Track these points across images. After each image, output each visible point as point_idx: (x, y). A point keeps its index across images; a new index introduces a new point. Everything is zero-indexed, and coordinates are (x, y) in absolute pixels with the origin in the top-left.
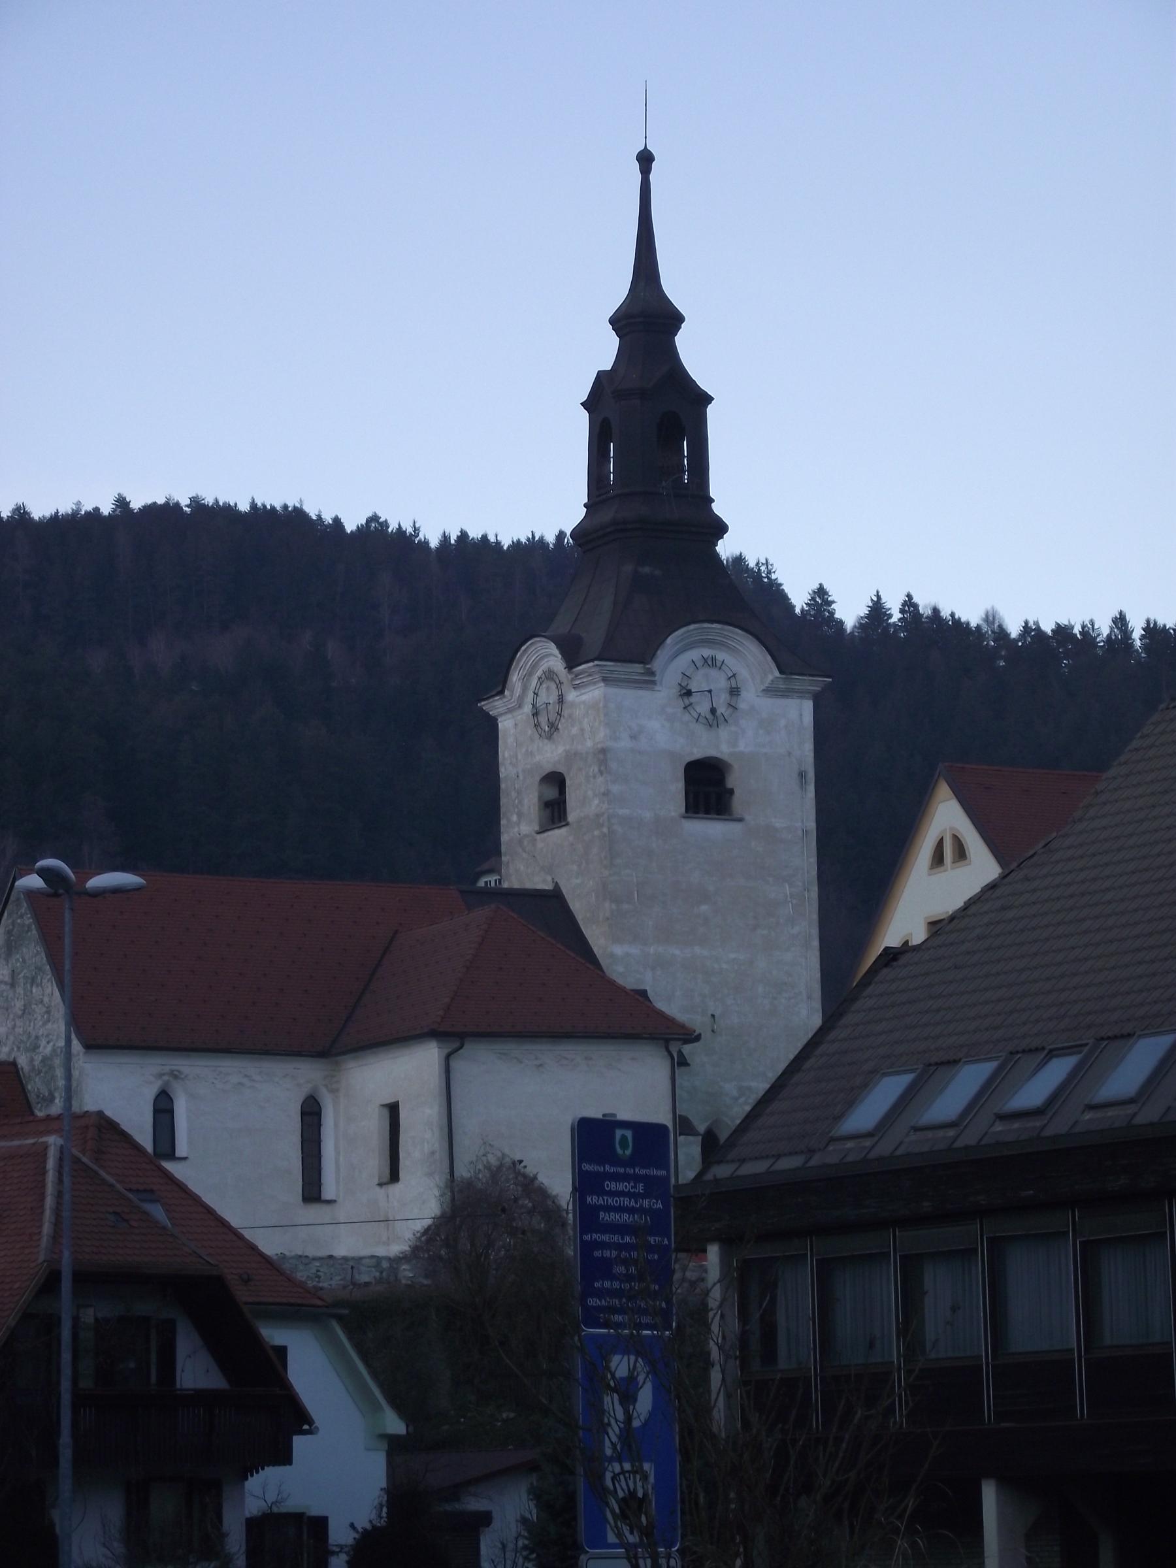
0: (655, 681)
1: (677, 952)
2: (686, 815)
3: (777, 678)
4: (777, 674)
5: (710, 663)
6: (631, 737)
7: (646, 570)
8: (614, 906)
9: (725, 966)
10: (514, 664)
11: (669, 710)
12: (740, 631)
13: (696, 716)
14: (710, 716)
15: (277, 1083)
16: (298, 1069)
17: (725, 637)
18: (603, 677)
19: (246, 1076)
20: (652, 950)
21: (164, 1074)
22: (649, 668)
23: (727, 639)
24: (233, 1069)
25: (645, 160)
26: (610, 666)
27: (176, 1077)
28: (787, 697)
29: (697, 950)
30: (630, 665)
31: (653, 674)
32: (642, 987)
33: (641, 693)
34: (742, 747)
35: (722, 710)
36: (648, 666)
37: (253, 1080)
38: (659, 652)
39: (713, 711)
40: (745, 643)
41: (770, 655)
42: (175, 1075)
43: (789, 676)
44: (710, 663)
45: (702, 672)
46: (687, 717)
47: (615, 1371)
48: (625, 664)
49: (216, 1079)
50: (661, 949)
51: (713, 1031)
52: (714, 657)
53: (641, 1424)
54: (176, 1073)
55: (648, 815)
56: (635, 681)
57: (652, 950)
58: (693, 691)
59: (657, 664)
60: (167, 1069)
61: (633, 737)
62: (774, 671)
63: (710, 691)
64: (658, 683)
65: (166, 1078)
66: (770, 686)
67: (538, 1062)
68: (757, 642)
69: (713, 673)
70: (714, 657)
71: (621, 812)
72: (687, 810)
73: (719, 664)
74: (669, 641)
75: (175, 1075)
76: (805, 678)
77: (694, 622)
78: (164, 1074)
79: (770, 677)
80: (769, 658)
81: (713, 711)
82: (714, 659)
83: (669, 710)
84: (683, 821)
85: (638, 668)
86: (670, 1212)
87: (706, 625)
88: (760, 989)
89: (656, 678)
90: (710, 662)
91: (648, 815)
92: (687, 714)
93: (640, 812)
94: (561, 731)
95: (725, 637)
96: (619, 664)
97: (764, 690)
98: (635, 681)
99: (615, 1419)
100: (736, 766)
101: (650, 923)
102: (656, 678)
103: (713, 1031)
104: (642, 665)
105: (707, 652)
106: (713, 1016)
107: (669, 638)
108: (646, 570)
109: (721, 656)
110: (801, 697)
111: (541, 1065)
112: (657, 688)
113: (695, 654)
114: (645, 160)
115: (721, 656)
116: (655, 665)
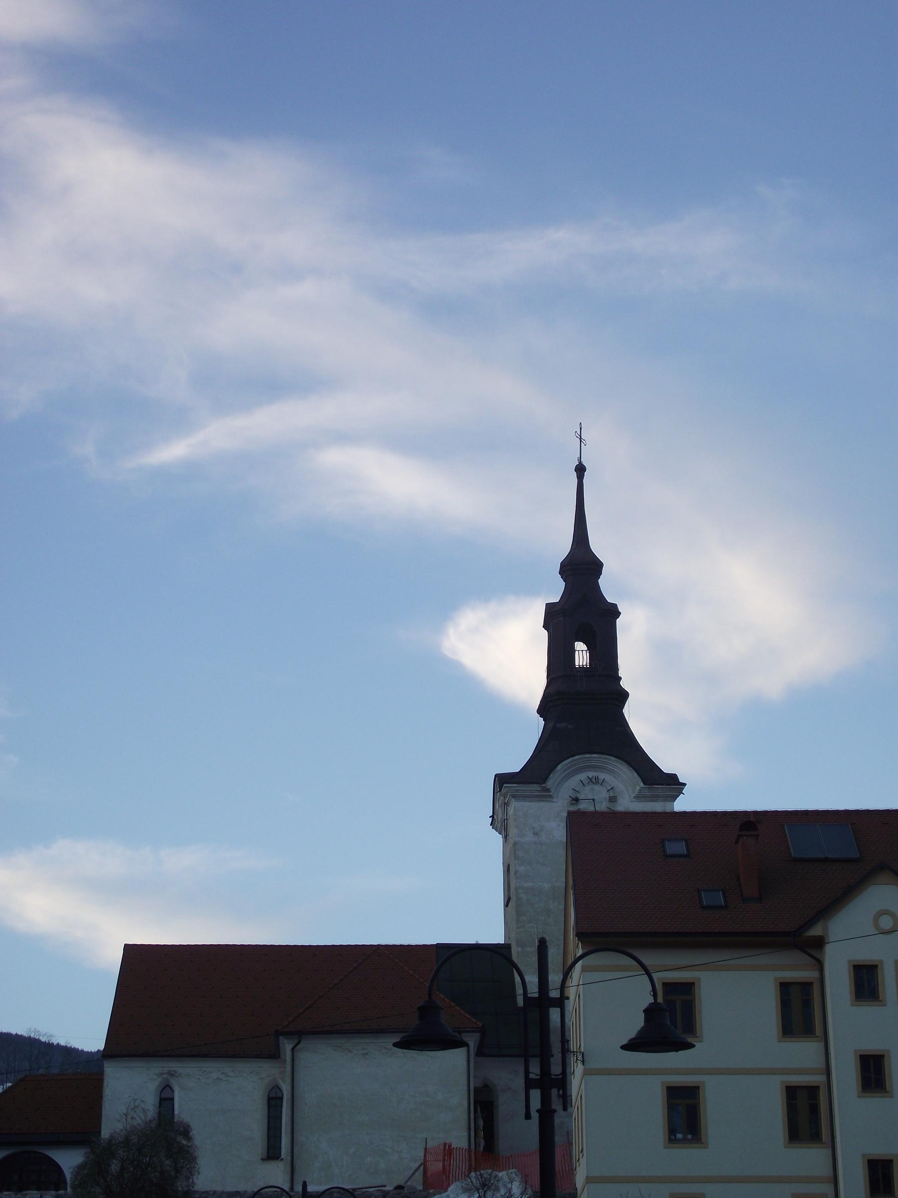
3: (642, 787)
4: (642, 785)
5: (594, 781)
6: (534, 834)
7: (562, 725)
8: (519, 949)
12: (613, 759)
15: (246, 1077)
16: (261, 1067)
17: (604, 763)
19: (223, 1073)
21: (163, 1074)
22: (544, 787)
24: (214, 1069)
25: (580, 470)
27: (172, 1075)
28: (654, 801)
30: (530, 785)
31: (548, 790)
33: (542, 804)
36: (543, 785)
37: (228, 1076)
38: (551, 775)
40: (618, 766)
41: (637, 773)
42: (172, 1074)
43: (652, 786)
44: (594, 781)
45: (588, 788)
48: (527, 785)
49: (201, 1076)
52: (597, 777)
54: (172, 1072)
55: (546, 886)
56: (537, 796)
60: (166, 1070)
61: (535, 834)
63: (593, 800)
65: (165, 1076)
66: (638, 794)
67: (364, 1052)
68: (626, 765)
69: (597, 788)
70: (597, 777)
71: (527, 885)
73: (600, 782)
74: (559, 767)
75: (172, 1074)
76: (664, 786)
77: (578, 754)
78: (163, 1074)
79: (638, 788)
80: (636, 774)
82: (597, 778)
85: (535, 787)
87: (587, 755)
89: (552, 794)
90: (595, 781)
91: (546, 886)
93: (541, 884)
95: (604, 763)
96: (521, 785)
97: (635, 797)
98: (537, 796)
102: (552, 794)
104: (538, 785)
105: (591, 774)
107: (560, 765)
108: (562, 725)
109: (602, 776)
110: (664, 801)
111: (366, 1054)
113: (583, 776)
114: (580, 470)
115: (602, 776)
116: (548, 784)
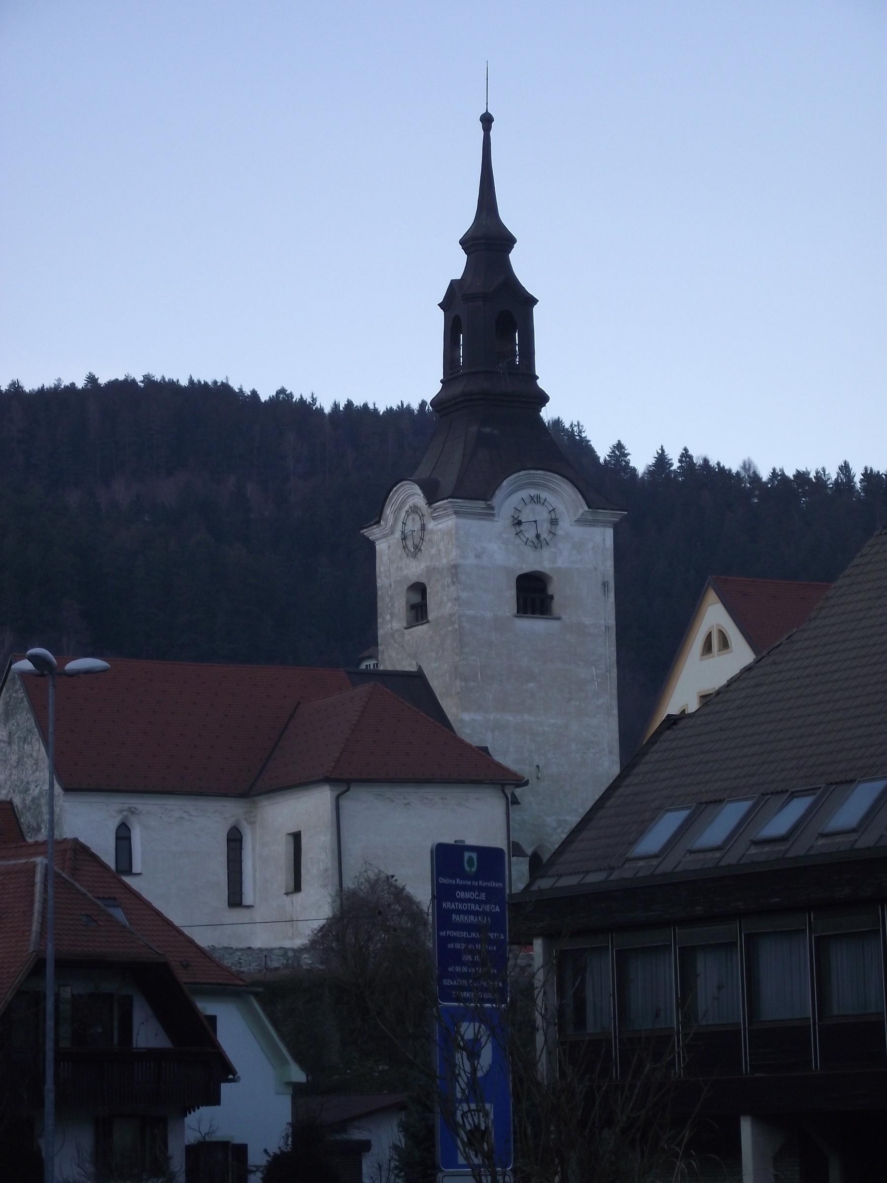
0: (494, 514)
1: (511, 718)
2: (518, 615)
3: (586, 511)
4: (586, 508)
5: (536, 500)
6: (476, 556)
7: (487, 430)
8: (463, 684)
9: (547, 729)
10: (388, 501)
11: (505, 536)
12: (558, 476)
13: (525, 540)
14: (535, 540)
15: (209, 817)
16: (225, 806)
17: (547, 480)
18: (455, 511)
19: (185, 812)
20: (492, 717)
21: (124, 811)
22: (490, 504)
23: (548, 482)
24: (176, 807)
25: (487, 120)
26: (460, 502)
27: (133, 813)
28: (594, 526)
29: (526, 716)
30: (475, 502)
31: (492, 508)
32: (484, 745)
33: (483, 522)
34: (559, 563)
35: (544, 535)
36: (488, 503)
37: (191, 815)
38: (497, 492)
39: (538, 536)
40: (562, 485)
41: (581, 494)
42: (132, 811)
43: (595, 510)
44: (536, 500)
45: (529, 507)
46: (518, 541)
47: (464, 1034)
48: (471, 501)
49: (163, 814)
50: (498, 716)
51: (538, 778)
52: (538, 495)
53: (483, 1074)
54: (132, 809)
55: (489, 615)
56: (479, 514)
57: (492, 717)
58: (522, 521)
59: (495, 501)
60: (126, 806)
61: (478, 556)
62: (584, 506)
63: (535, 521)
64: (496, 516)
65: (125, 813)
66: (581, 517)
67: (406, 802)
68: (571, 485)
69: (538, 507)
70: (538, 495)
71: (469, 612)
72: (518, 611)
73: (542, 501)
74: (505, 483)
75: (132, 811)
76: (607, 511)
77: (524, 470)
78: (124, 811)
79: (581, 511)
80: (580, 496)
81: (538, 536)
82: (538, 497)
83: (505, 536)
84: (515, 619)
85: (481, 504)
86: (505, 914)
87: (532, 472)
88: (573, 746)
89: (495, 512)
90: (535, 500)
91: (489, 615)
92: (518, 539)
93: (483, 612)
94: (423, 552)
95: (547, 480)
96: (467, 501)
97: (576, 521)
98: (479, 514)
99: (464, 1070)
100: (555, 578)
101: (491, 696)
102: (495, 512)
103: (538, 778)
104: (484, 502)
105: (533, 492)
106: (538, 766)
107: (505, 481)
108: (487, 430)
109: (544, 495)
110: (604, 526)
111: (408, 804)
112: (495, 519)
113: (524, 494)
114: (487, 120)
115: (544, 495)
116: (494, 501)
